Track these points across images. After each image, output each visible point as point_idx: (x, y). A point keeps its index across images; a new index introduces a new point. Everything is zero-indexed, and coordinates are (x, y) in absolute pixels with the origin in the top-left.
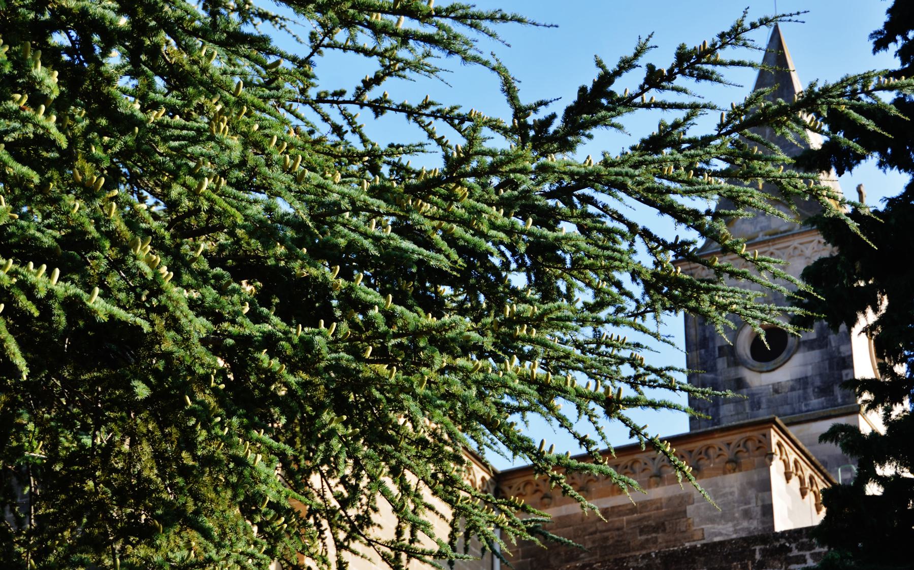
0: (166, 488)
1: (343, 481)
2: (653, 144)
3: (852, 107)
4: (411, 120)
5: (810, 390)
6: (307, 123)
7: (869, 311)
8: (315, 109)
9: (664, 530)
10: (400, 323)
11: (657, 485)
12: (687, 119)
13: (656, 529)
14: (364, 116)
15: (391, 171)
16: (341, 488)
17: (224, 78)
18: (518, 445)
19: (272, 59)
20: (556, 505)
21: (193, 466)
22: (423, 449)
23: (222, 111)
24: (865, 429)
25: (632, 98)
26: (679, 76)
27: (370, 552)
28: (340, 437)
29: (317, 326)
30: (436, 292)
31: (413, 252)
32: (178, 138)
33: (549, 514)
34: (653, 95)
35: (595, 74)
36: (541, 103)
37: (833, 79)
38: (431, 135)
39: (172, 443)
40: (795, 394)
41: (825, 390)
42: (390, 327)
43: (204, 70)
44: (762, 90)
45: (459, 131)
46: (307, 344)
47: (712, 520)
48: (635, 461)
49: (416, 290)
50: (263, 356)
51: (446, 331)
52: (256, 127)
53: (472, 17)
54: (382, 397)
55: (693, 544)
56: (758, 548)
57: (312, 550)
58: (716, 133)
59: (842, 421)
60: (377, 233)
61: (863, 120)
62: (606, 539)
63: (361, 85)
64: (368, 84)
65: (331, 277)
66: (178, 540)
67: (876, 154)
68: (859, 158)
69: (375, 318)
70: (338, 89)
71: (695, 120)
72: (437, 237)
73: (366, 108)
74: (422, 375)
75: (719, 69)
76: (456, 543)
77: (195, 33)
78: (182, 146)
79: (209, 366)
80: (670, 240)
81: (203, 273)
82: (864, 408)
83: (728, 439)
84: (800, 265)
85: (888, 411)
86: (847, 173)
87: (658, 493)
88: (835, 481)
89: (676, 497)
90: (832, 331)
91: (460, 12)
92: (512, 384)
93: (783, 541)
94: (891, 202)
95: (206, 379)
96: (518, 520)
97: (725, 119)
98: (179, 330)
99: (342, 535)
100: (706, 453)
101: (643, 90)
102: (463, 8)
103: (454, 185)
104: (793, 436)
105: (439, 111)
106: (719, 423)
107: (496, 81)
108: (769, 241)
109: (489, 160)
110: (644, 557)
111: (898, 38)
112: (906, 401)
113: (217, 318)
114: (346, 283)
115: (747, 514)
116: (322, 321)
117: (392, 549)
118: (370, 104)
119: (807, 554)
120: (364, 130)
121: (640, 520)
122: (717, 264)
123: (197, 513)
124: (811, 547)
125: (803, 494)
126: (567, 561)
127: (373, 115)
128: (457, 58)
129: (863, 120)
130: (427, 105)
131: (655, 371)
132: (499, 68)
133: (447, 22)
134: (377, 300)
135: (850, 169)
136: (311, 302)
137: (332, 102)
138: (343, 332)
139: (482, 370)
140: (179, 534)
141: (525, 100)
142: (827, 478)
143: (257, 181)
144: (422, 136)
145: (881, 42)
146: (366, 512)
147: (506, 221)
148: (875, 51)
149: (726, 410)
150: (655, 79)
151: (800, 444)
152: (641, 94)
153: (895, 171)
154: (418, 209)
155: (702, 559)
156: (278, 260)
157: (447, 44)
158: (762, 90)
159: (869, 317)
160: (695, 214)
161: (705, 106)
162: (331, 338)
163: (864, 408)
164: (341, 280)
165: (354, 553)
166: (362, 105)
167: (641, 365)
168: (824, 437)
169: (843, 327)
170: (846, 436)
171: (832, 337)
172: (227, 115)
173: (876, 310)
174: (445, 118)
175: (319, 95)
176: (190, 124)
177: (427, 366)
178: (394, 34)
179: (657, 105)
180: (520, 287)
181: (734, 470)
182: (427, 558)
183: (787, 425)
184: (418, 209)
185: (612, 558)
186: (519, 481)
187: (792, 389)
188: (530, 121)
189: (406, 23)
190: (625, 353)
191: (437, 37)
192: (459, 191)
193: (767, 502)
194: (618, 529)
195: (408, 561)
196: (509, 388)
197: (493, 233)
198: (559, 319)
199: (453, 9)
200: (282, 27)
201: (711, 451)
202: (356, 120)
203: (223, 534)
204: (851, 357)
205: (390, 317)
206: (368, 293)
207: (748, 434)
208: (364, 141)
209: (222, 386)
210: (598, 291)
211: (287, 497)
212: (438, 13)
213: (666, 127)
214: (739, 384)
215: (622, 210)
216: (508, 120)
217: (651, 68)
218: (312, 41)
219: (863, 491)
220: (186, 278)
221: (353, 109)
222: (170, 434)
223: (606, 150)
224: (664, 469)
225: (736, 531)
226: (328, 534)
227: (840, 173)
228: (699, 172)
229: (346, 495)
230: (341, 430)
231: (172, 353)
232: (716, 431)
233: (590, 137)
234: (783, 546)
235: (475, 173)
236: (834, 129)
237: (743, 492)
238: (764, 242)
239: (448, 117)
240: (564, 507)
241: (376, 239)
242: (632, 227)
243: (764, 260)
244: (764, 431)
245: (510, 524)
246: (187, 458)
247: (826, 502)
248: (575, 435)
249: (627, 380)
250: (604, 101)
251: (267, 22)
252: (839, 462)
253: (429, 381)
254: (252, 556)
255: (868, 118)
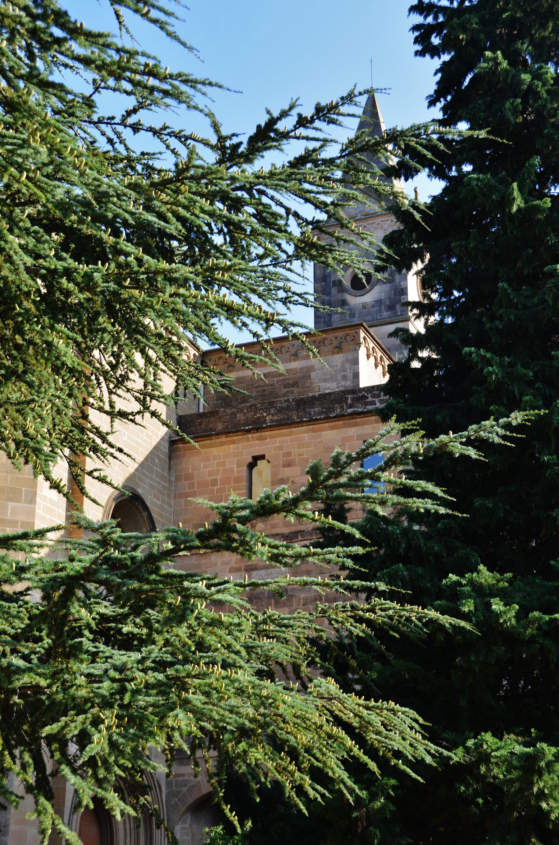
0: (6, 357)
1: (113, 354)
2: (300, 161)
3: (417, 143)
4: (156, 136)
5: (383, 307)
6: (91, 136)
7: (419, 262)
8: (97, 127)
9: (298, 386)
10: (146, 266)
11: (295, 360)
12: (321, 147)
13: (293, 385)
14: (127, 133)
15: (143, 169)
16: (112, 359)
17: (37, 108)
18: (214, 339)
19: (70, 97)
20: (236, 371)
21: (23, 344)
22: (159, 339)
23: (37, 128)
24: (413, 331)
25: (288, 133)
26: (317, 121)
27: (128, 396)
28: (109, 332)
29: (96, 264)
30: (170, 245)
31: (155, 223)
32: (11, 144)
33: (232, 376)
34: (301, 131)
35: (266, 118)
36: (234, 135)
37: (406, 126)
38: (168, 147)
39: (10, 330)
40: (374, 309)
41: (391, 307)
42: (141, 268)
43: (25, 102)
44: (363, 130)
45: (185, 145)
46: (88, 277)
47: (325, 381)
48: (283, 347)
49: (157, 243)
50: (64, 280)
51: (173, 273)
52: (59, 140)
53: (191, 81)
54: (135, 307)
55: (313, 394)
56: (350, 396)
57: (93, 394)
58: (339, 155)
59: (400, 325)
60: (134, 210)
61: (425, 152)
62: (264, 391)
63: (125, 114)
64: (129, 113)
65: (105, 236)
66: (14, 387)
67: (427, 170)
68: (417, 171)
69: (131, 262)
70: (111, 115)
71: (326, 148)
72: (169, 215)
73: (128, 128)
74: (159, 297)
75: (340, 118)
76: (179, 392)
77: (21, 77)
78: (14, 149)
79: (30, 286)
80: (310, 219)
81: (27, 229)
82: (413, 319)
83: (336, 334)
84: (381, 234)
85: (427, 320)
86: (410, 180)
87: (295, 365)
88: (394, 359)
89: (305, 367)
90: (397, 273)
91: (184, 78)
92: (211, 307)
93: (363, 393)
94: (434, 198)
95: (28, 294)
96: (215, 379)
97: (344, 147)
98: (12, 263)
99: (112, 386)
100: (323, 343)
101: (296, 128)
102: (186, 75)
103: (180, 184)
104: (372, 334)
105: (172, 132)
106: (331, 325)
107: (208, 121)
108: (364, 219)
109: (201, 171)
110: (285, 401)
111: (442, 99)
112: (437, 315)
113: (37, 256)
114: (114, 240)
115: (344, 378)
116: (100, 262)
117: (141, 394)
118: (130, 126)
119: (377, 400)
120: (127, 142)
121: (284, 380)
122: (336, 234)
123: (25, 372)
124: (379, 396)
125: (376, 366)
126: (242, 403)
127: (132, 133)
128: (184, 106)
129: (425, 152)
130: (165, 128)
131: (297, 295)
132: (210, 114)
133: (176, 83)
134: (133, 251)
135: (412, 178)
136: (94, 248)
137: (107, 123)
138: (112, 269)
139: (195, 297)
140: (14, 383)
141: (225, 132)
142: (390, 358)
143: (59, 175)
144: (163, 148)
145: (432, 103)
146: (126, 372)
147: (211, 208)
148: (429, 107)
149: (335, 318)
150: (302, 122)
151: (376, 338)
152: (295, 130)
153: (437, 180)
154: (157, 199)
155: (318, 402)
156: (73, 223)
157: (177, 96)
158: (363, 130)
159: (418, 266)
160: (325, 204)
161: (331, 141)
162: (105, 272)
163: (413, 319)
164: (111, 238)
165: (119, 396)
166: (125, 126)
167: (289, 291)
168: (391, 335)
169: (404, 271)
170: (403, 334)
171: (397, 277)
172: (41, 131)
173: (423, 262)
174: (176, 137)
175: (99, 119)
176: (18, 135)
177: (161, 292)
178: (145, 87)
179: (303, 138)
180: (219, 245)
181: (339, 353)
182: (161, 400)
183: (369, 327)
184: (157, 199)
185: (267, 401)
186: (215, 357)
187: (373, 306)
188: (228, 144)
189: (152, 82)
190: (281, 284)
191: (171, 92)
192: (182, 187)
193: (356, 371)
194: (271, 385)
195: (151, 402)
196: (210, 309)
197: (202, 215)
198: (240, 269)
199: (180, 75)
200: (77, 73)
201: (326, 342)
202: (122, 135)
203: (41, 384)
204: (406, 288)
205: (140, 261)
206: (127, 246)
207: (347, 332)
208: (127, 149)
209: (38, 299)
210: (266, 249)
211: (78, 365)
212: (171, 76)
213: (309, 151)
214: (344, 303)
215: (282, 200)
216: (214, 140)
217: (300, 116)
218: (94, 85)
219: (409, 365)
220: (16, 231)
221: (120, 128)
222: (9, 324)
223: (274, 162)
224: (299, 351)
225: (338, 387)
226: (103, 385)
227: (406, 180)
228: (327, 179)
229: (114, 362)
230: (110, 327)
231: (7, 277)
232: (329, 330)
233: (263, 157)
234: (363, 396)
235: (192, 178)
236: (404, 153)
237: (343, 365)
238: (360, 220)
239: (177, 136)
240: (241, 372)
241: (132, 214)
242: (288, 210)
243: (363, 234)
244: (356, 331)
245: (211, 382)
246: (19, 339)
247: (389, 372)
248: (250, 331)
249: (281, 300)
250: (272, 135)
251: (68, 69)
252: (398, 348)
253: (163, 301)
254: (59, 397)
255: (428, 151)
